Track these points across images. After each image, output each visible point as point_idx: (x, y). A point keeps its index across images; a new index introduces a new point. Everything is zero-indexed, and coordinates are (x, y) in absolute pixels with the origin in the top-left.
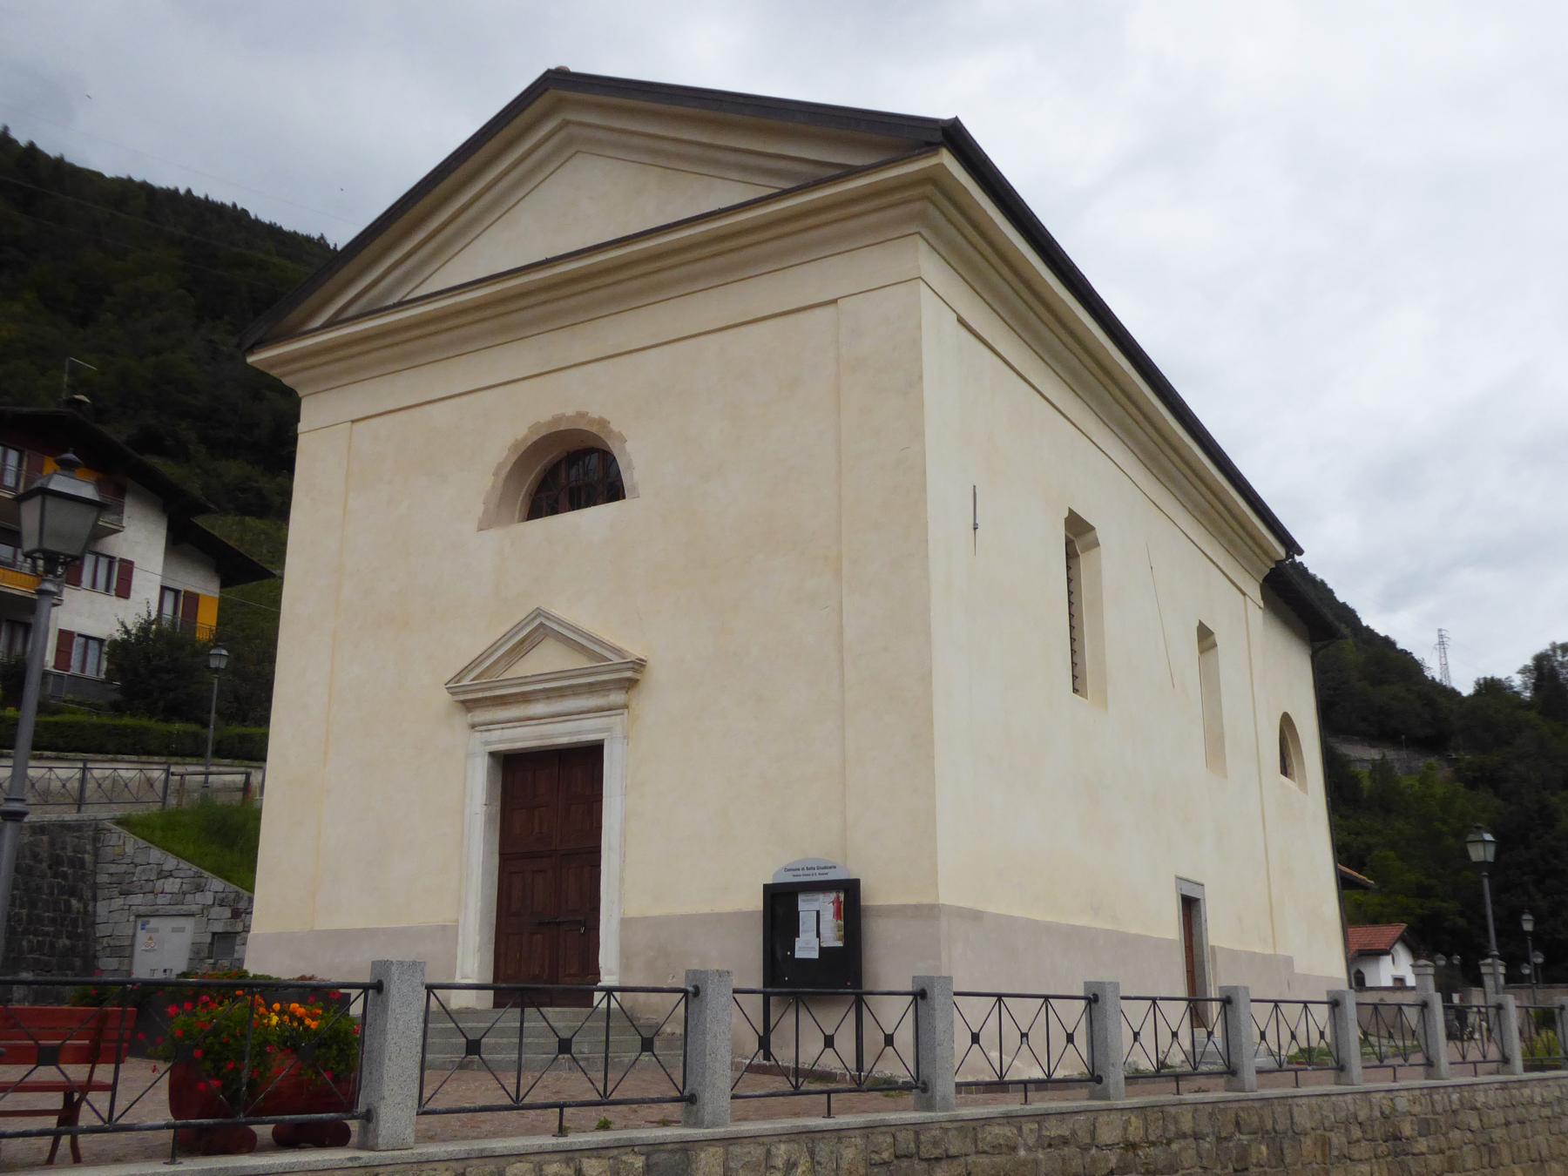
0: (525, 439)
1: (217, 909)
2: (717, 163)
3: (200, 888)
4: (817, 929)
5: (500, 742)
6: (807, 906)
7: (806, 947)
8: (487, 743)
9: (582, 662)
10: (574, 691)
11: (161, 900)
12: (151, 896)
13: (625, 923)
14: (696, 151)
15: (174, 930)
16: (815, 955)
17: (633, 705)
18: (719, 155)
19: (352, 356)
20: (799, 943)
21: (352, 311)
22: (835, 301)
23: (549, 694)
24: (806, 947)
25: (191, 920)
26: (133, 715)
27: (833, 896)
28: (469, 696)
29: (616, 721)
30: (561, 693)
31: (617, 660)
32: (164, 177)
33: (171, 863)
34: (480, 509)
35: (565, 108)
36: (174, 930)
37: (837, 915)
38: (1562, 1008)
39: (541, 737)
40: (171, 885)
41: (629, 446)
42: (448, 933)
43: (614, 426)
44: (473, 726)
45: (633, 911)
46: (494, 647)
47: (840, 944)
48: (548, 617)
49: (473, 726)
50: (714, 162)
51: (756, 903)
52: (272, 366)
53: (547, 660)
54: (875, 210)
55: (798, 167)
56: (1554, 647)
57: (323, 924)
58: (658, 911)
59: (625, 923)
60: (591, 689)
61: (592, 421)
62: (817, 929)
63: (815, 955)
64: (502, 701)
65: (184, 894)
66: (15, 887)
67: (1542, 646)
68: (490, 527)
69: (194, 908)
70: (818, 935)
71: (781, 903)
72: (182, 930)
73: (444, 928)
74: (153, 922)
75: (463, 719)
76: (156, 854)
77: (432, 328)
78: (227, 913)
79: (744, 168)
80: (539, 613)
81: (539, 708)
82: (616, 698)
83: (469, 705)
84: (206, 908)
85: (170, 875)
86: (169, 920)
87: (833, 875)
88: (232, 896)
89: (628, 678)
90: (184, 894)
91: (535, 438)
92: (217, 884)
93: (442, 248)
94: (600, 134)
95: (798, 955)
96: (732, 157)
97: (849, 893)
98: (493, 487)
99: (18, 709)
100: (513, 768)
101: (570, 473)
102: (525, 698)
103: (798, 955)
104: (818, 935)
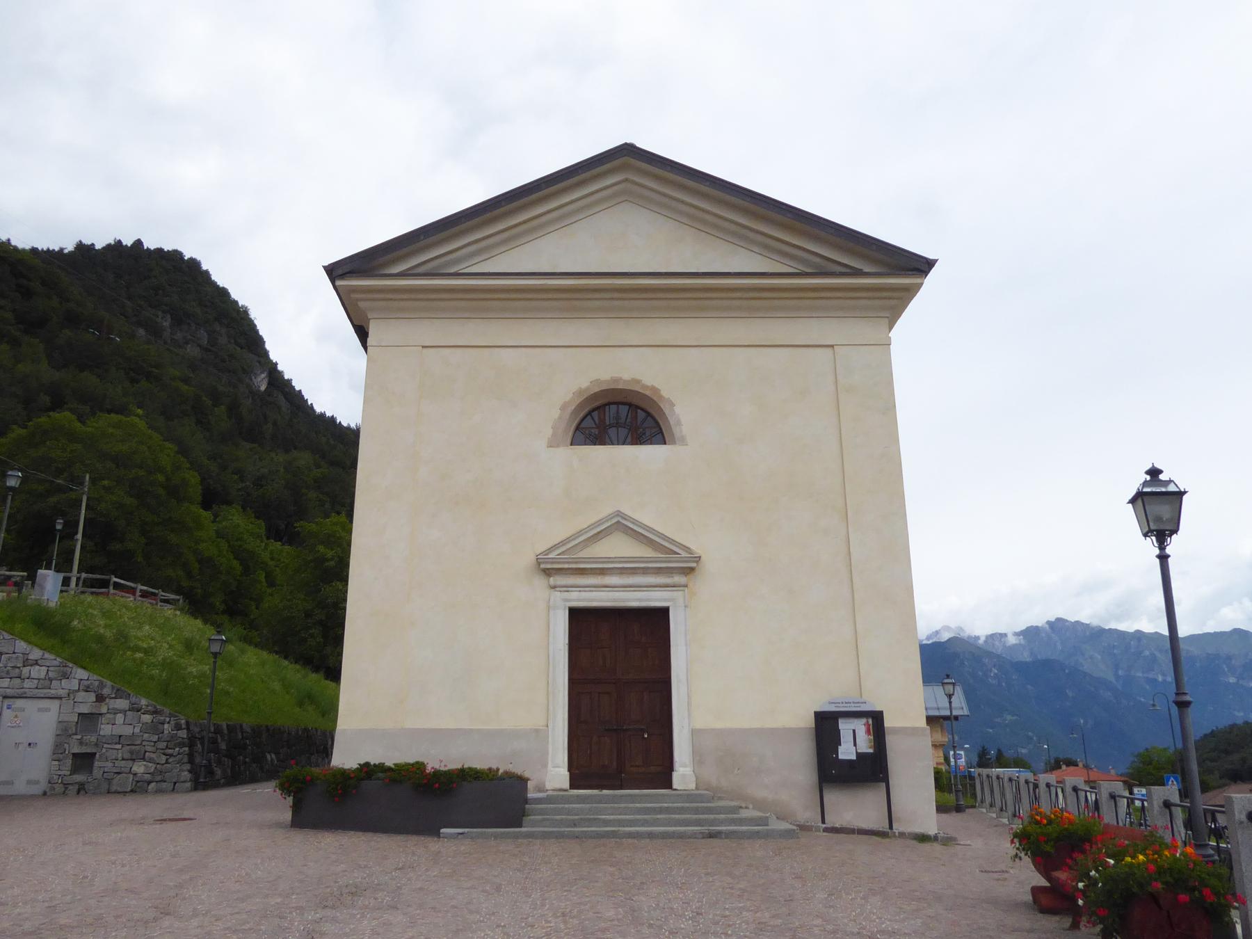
0: (587, 389)
1: (82, 694)
2: (746, 239)
3: (65, 676)
4: (853, 742)
5: (579, 600)
6: (845, 726)
7: (846, 752)
8: (566, 600)
9: (647, 552)
10: (645, 571)
11: (27, 684)
12: (18, 681)
13: (695, 733)
14: (733, 227)
15: (40, 710)
16: (854, 757)
17: (690, 585)
20: (841, 749)
21: (420, 270)
22: (832, 346)
23: (622, 572)
24: (846, 752)
25: (57, 702)
26: (76, 533)
27: (864, 720)
28: (549, 566)
29: (678, 595)
30: (633, 571)
31: (684, 554)
33: (36, 654)
34: (550, 432)
35: (627, 170)
36: (40, 710)
37: (868, 732)
39: (615, 600)
40: (38, 672)
41: (677, 409)
42: (539, 734)
43: (664, 393)
44: (554, 587)
45: (698, 725)
46: (580, 533)
47: (871, 751)
48: (625, 517)
49: (554, 587)
50: (742, 237)
51: (810, 722)
53: (618, 548)
54: (869, 298)
55: (817, 260)
57: (410, 724)
58: (719, 725)
59: (695, 733)
60: (658, 571)
62: (853, 742)
63: (854, 757)
64: (582, 572)
65: (51, 680)
68: (558, 446)
69: (62, 693)
70: (855, 745)
71: (826, 725)
72: (48, 710)
73: (537, 731)
74: (19, 703)
75: (540, 582)
76: (21, 646)
78: (92, 697)
79: (766, 247)
80: (619, 514)
82: (678, 579)
83: (548, 573)
84: (71, 693)
85: (36, 663)
86: (35, 702)
88: (97, 683)
89: (685, 567)
90: (51, 680)
91: (597, 389)
92: (81, 674)
93: (511, 239)
95: (841, 757)
96: (760, 238)
97: (876, 719)
98: (560, 418)
99: (1005, 635)
101: (619, 417)
102: (602, 572)
103: (841, 757)
104: (855, 745)
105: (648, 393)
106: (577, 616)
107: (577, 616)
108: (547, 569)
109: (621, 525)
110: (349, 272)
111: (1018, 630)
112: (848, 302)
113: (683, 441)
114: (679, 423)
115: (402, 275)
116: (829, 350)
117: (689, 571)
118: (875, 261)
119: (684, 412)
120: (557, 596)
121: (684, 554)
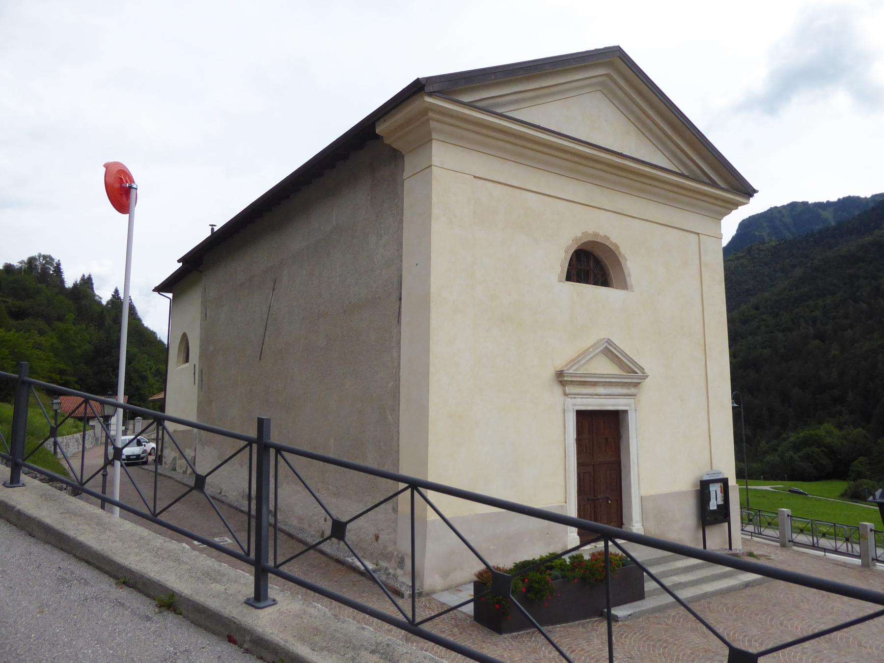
0: (620, 252)
7: (713, 506)
8: (574, 405)
10: (617, 384)
18: (669, 143)
19: (488, 136)
20: (711, 503)
21: (479, 104)
22: (698, 234)
29: (631, 401)
32: (755, 213)
35: (612, 71)
38: (274, 602)
41: (628, 263)
50: (661, 142)
52: (433, 111)
56: (40, 256)
61: (612, 243)
66: (759, 479)
67: (34, 254)
75: (558, 390)
77: (546, 150)
80: (609, 342)
81: (601, 390)
82: (633, 390)
87: (721, 477)
93: (538, 97)
94: (620, 93)
96: (673, 147)
100: (588, 421)
101: (591, 265)
102: (595, 384)
105: (613, 248)
106: (582, 415)
107: (582, 415)
108: (561, 378)
109: (610, 352)
110: (438, 92)
111: (158, 283)
112: (616, 177)
113: (624, 285)
114: (629, 275)
115: (470, 105)
116: (696, 236)
117: (636, 385)
118: (725, 180)
119: (634, 265)
120: (569, 401)
121: (640, 374)
